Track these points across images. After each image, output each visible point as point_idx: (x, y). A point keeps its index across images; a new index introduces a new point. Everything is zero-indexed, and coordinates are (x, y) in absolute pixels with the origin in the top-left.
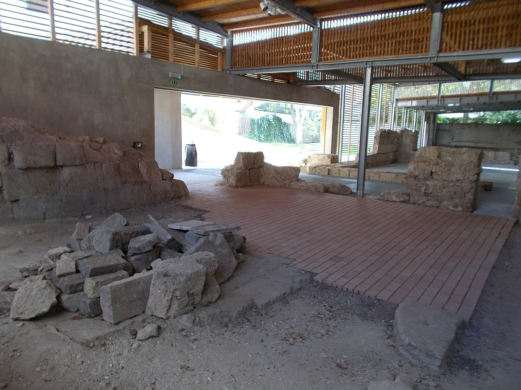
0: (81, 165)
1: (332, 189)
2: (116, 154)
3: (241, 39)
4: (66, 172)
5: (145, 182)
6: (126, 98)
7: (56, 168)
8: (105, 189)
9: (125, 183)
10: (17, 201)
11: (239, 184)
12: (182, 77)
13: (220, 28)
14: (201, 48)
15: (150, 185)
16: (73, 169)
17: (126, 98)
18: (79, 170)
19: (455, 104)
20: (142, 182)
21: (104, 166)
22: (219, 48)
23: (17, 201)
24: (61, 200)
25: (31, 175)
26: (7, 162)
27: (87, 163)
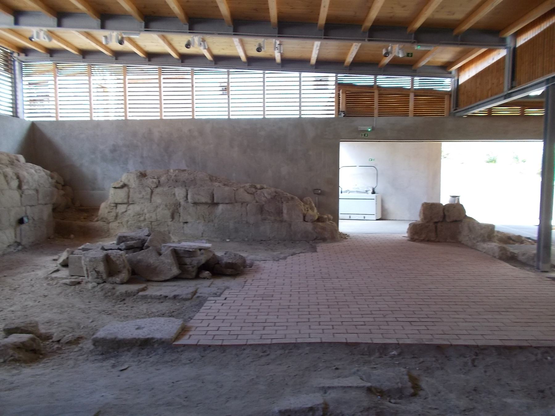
0: (232, 203)
1: (521, 258)
2: (265, 197)
3: (464, 77)
4: (221, 207)
5: (285, 221)
6: (310, 153)
7: (214, 204)
8: (247, 223)
9: (265, 220)
10: (186, 223)
11: (416, 237)
12: (373, 129)
13: (440, 71)
14: (415, 96)
15: (290, 225)
16: (225, 205)
17: (310, 153)
18: (229, 207)
19: (523, 112)
20: (282, 221)
21: (249, 205)
22: (446, 91)
23: (186, 223)
24: (214, 226)
25: (199, 207)
26: (185, 199)
27: (236, 202)
